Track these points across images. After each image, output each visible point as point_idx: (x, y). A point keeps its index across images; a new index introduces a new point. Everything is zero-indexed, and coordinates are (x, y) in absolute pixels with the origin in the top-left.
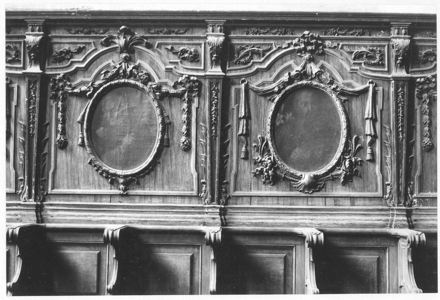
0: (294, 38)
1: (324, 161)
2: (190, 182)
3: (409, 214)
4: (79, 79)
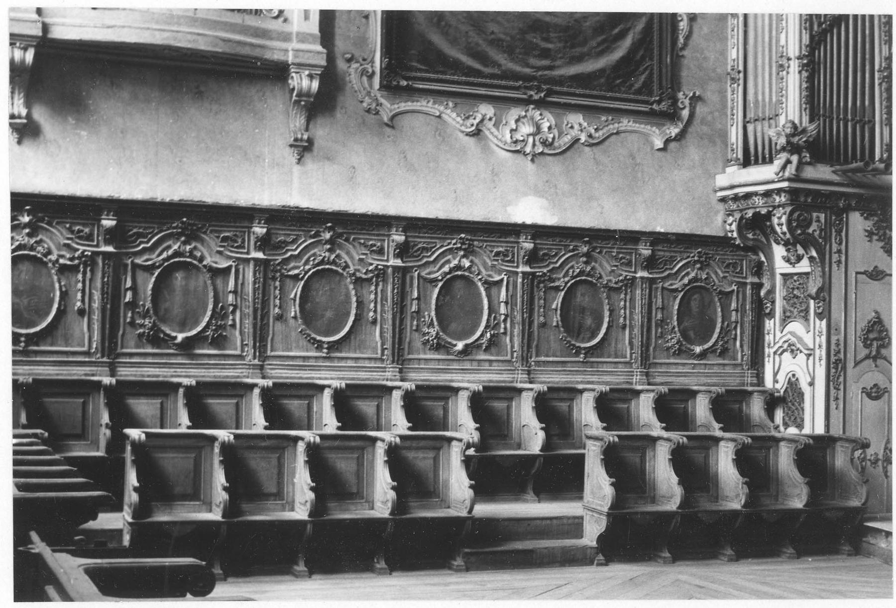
0: (453, 239)
1: (473, 333)
2: (375, 348)
3: (529, 373)
4: (292, 265)
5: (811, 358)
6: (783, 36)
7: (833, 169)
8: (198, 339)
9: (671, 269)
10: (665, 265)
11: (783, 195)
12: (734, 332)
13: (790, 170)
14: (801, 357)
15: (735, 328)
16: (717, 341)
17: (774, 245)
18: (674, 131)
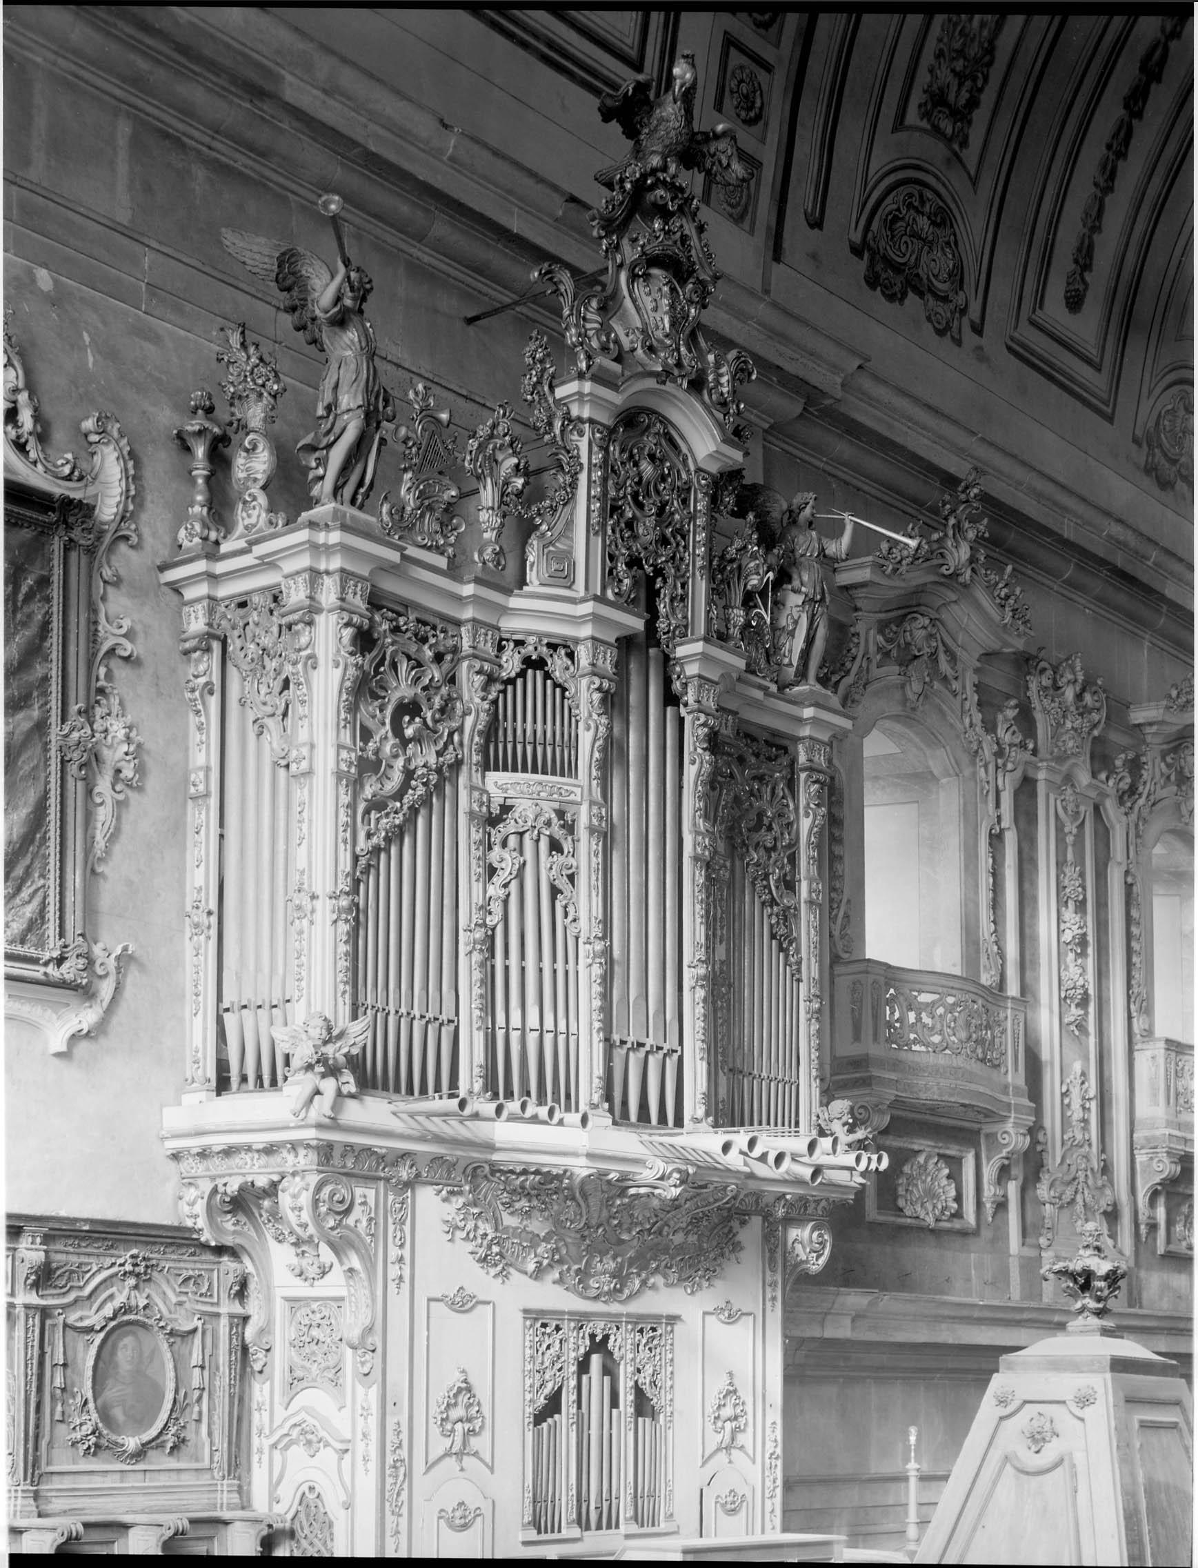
5: (348, 1456)
6: (302, 852)
7: (392, 1107)
8: (154, 1444)
9: (81, 1288)
10: (69, 1279)
11: (302, 1152)
12: (196, 1409)
13: (323, 1106)
14: (327, 1456)
15: (200, 1399)
16: (166, 1427)
17: (272, 1243)
18: (88, 1017)
